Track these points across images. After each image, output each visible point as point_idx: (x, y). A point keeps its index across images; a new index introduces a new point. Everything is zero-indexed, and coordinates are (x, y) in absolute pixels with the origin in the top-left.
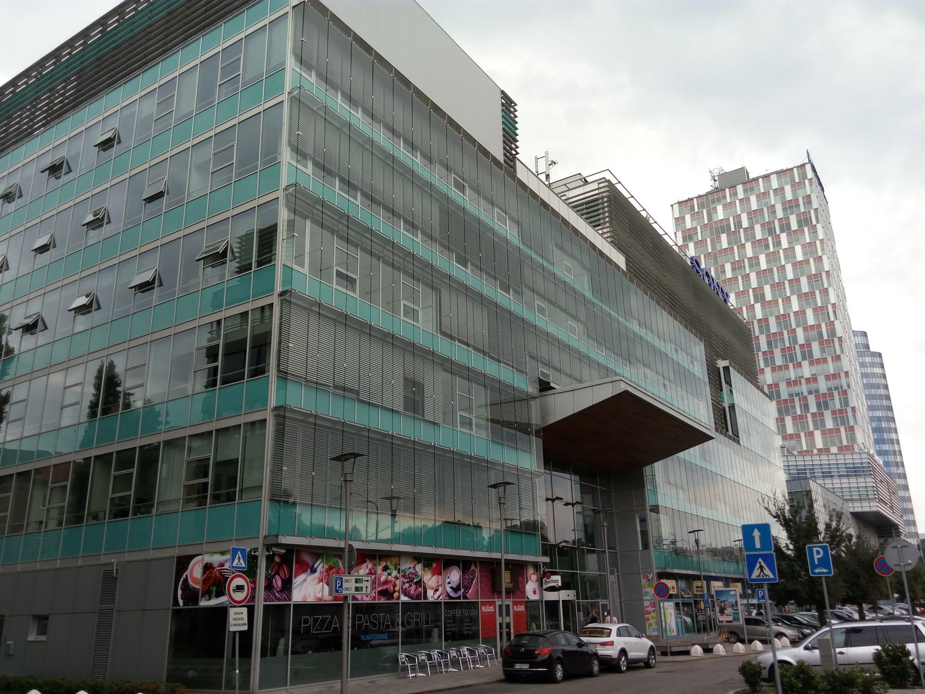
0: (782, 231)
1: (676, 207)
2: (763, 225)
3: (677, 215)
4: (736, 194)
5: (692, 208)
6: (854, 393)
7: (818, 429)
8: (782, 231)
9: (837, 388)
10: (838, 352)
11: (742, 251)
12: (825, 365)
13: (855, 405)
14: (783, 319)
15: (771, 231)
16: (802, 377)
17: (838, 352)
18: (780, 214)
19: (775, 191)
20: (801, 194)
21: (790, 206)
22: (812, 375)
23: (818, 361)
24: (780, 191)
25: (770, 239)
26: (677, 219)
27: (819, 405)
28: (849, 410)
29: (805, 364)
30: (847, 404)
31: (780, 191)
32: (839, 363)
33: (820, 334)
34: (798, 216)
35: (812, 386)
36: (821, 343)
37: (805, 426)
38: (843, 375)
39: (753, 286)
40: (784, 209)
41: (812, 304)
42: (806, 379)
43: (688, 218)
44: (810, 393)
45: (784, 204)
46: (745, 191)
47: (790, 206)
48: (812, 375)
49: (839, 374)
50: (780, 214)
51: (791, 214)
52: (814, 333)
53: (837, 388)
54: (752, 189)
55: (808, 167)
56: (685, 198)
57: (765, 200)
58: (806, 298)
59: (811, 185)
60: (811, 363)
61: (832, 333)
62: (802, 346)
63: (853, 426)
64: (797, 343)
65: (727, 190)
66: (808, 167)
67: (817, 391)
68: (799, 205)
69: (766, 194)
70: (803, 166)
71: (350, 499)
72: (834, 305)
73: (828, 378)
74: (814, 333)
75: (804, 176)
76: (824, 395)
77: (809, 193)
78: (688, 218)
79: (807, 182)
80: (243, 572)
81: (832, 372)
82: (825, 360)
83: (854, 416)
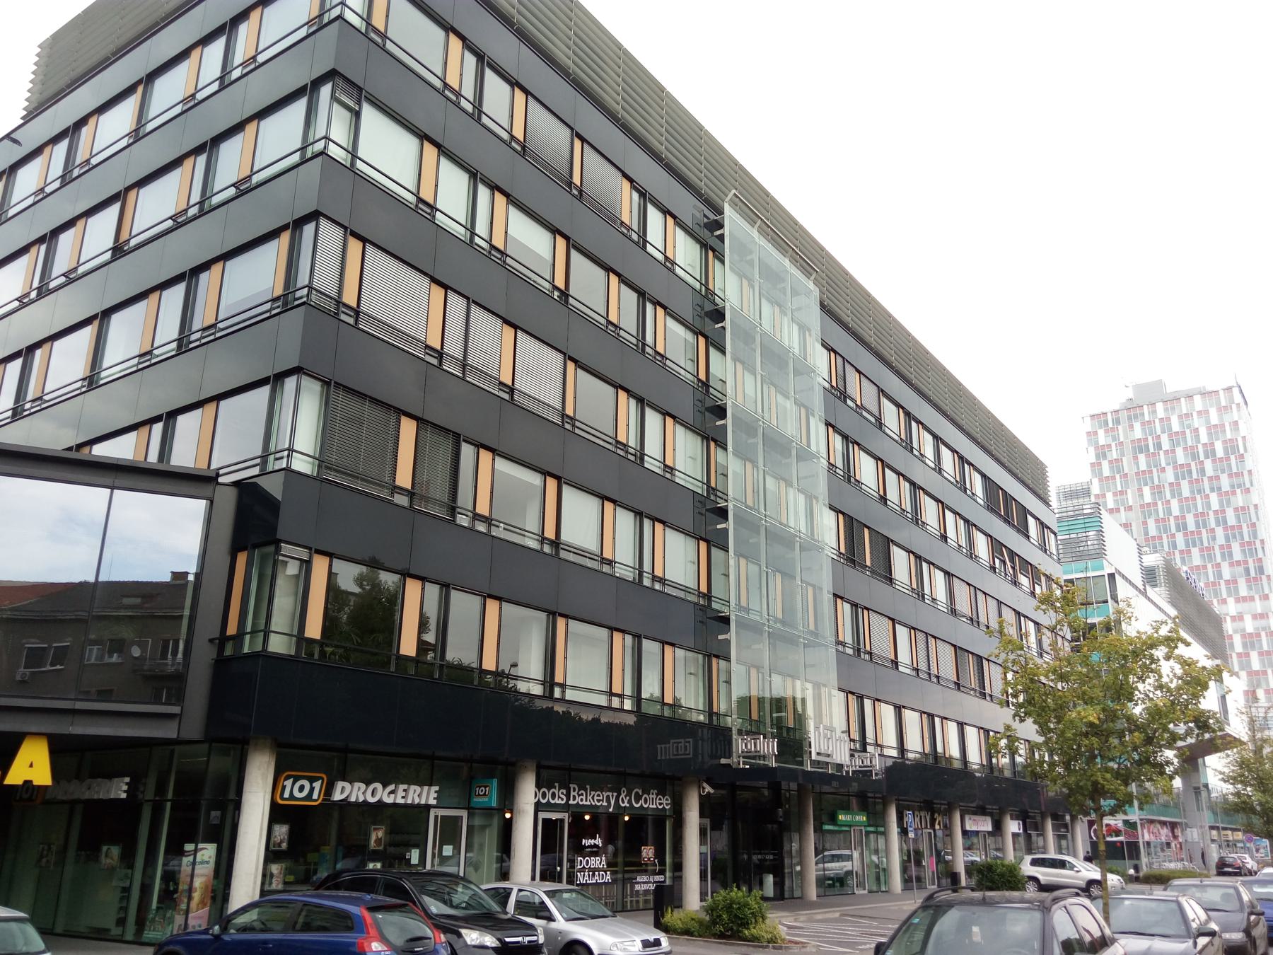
0: (1207, 457)
1: (1088, 419)
2: (1185, 449)
3: (1094, 460)
4: (1154, 412)
5: (1106, 423)
6: (1263, 526)
7: (1231, 596)
8: (1207, 457)
9: (1264, 629)
10: (1254, 520)
11: (1162, 475)
12: (1252, 603)
13: (1264, 537)
14: (1201, 519)
15: (1195, 456)
16: (1227, 614)
17: (1267, 591)
18: (1204, 438)
19: (1200, 413)
20: (1227, 419)
21: (1214, 430)
22: (1238, 613)
23: (1245, 599)
24: (1204, 413)
25: (1193, 464)
26: (1092, 465)
27: (1245, 645)
28: (1258, 543)
29: (1231, 601)
30: (1255, 536)
31: (1204, 413)
32: (1266, 602)
33: (1247, 571)
34: (1224, 442)
35: (1238, 624)
36: (1248, 581)
37: (1211, 557)
38: (1246, 473)
39: (1174, 514)
40: (1210, 434)
41: (1263, 684)
42: (1231, 617)
43: (1101, 433)
44: (1235, 631)
45: (1209, 428)
46: (1166, 410)
47: (1214, 430)
48: (1238, 613)
49: (1267, 614)
50: (1204, 438)
51: (1216, 440)
52: (1241, 569)
53: (1239, 486)
54: (1173, 409)
55: (1236, 391)
56: (1098, 412)
57: (1188, 422)
58: (1225, 497)
59: (1239, 411)
60: (1238, 600)
61: (1261, 570)
62: (1216, 512)
63: (1267, 595)
64: (1222, 578)
65: (1145, 407)
66: (1236, 391)
67: (1244, 630)
68: (1225, 431)
69: (1188, 416)
70: (1230, 389)
71: (534, 539)
72: (1244, 438)
73: (1255, 617)
74: (1241, 569)
75: (1231, 400)
76: (1251, 635)
77: (1236, 419)
78: (1101, 433)
79: (1234, 406)
80: (347, 797)
81: (1259, 611)
82: (1252, 599)
83: (1257, 513)
